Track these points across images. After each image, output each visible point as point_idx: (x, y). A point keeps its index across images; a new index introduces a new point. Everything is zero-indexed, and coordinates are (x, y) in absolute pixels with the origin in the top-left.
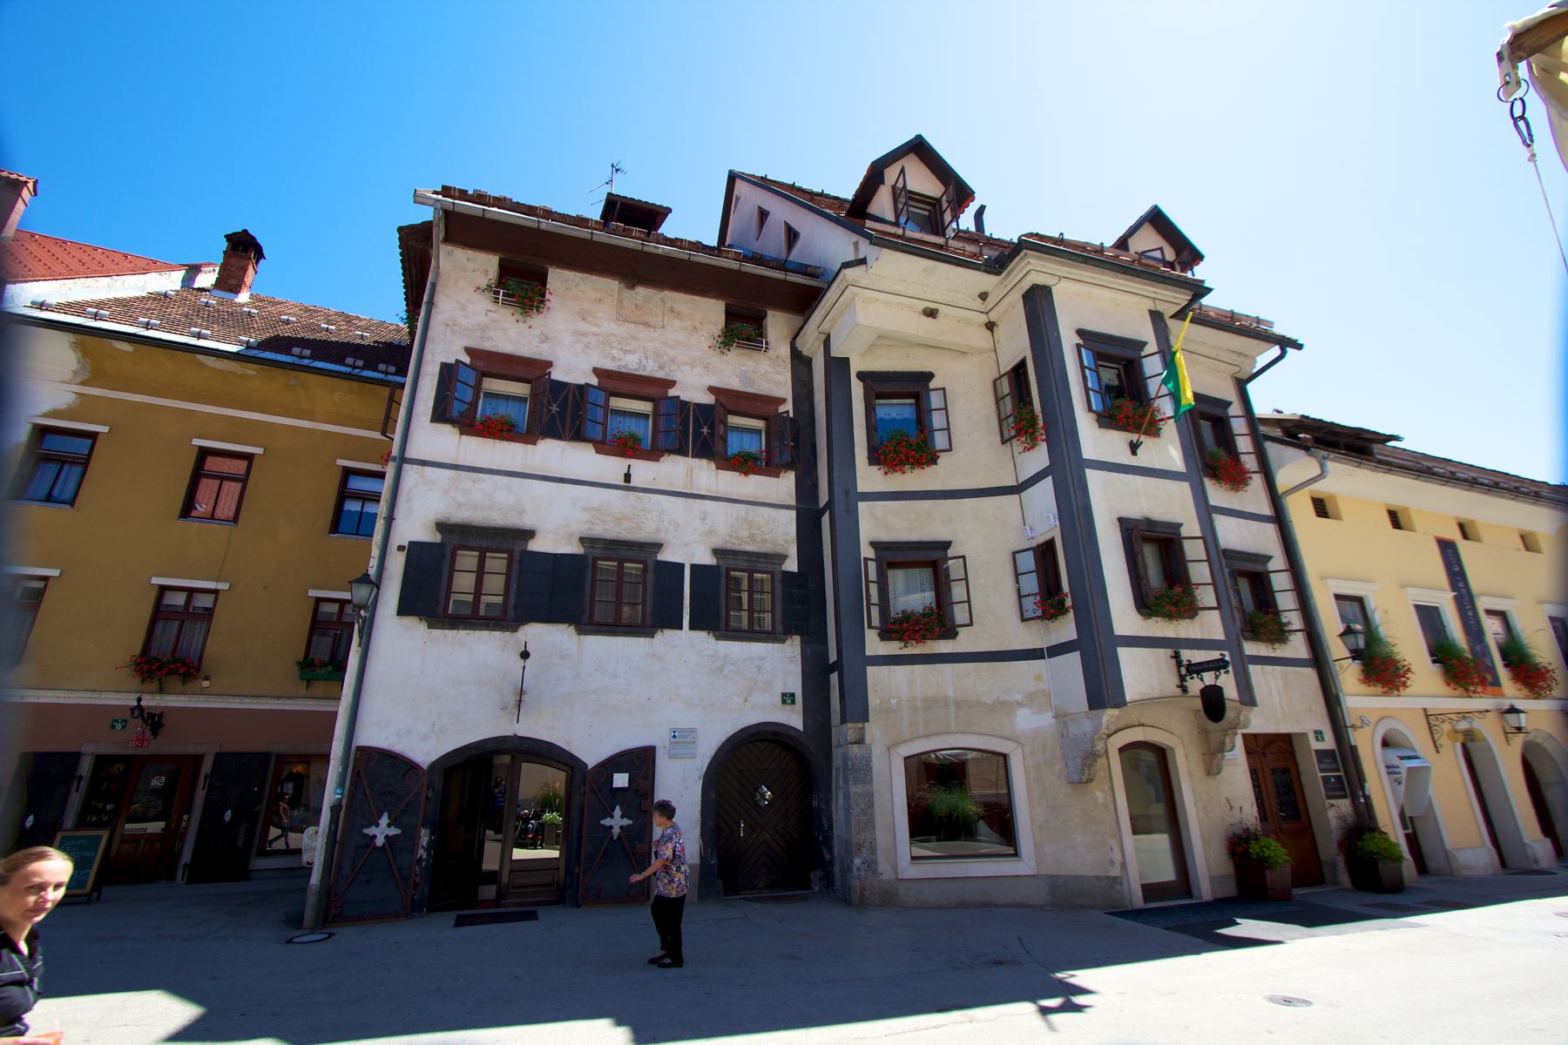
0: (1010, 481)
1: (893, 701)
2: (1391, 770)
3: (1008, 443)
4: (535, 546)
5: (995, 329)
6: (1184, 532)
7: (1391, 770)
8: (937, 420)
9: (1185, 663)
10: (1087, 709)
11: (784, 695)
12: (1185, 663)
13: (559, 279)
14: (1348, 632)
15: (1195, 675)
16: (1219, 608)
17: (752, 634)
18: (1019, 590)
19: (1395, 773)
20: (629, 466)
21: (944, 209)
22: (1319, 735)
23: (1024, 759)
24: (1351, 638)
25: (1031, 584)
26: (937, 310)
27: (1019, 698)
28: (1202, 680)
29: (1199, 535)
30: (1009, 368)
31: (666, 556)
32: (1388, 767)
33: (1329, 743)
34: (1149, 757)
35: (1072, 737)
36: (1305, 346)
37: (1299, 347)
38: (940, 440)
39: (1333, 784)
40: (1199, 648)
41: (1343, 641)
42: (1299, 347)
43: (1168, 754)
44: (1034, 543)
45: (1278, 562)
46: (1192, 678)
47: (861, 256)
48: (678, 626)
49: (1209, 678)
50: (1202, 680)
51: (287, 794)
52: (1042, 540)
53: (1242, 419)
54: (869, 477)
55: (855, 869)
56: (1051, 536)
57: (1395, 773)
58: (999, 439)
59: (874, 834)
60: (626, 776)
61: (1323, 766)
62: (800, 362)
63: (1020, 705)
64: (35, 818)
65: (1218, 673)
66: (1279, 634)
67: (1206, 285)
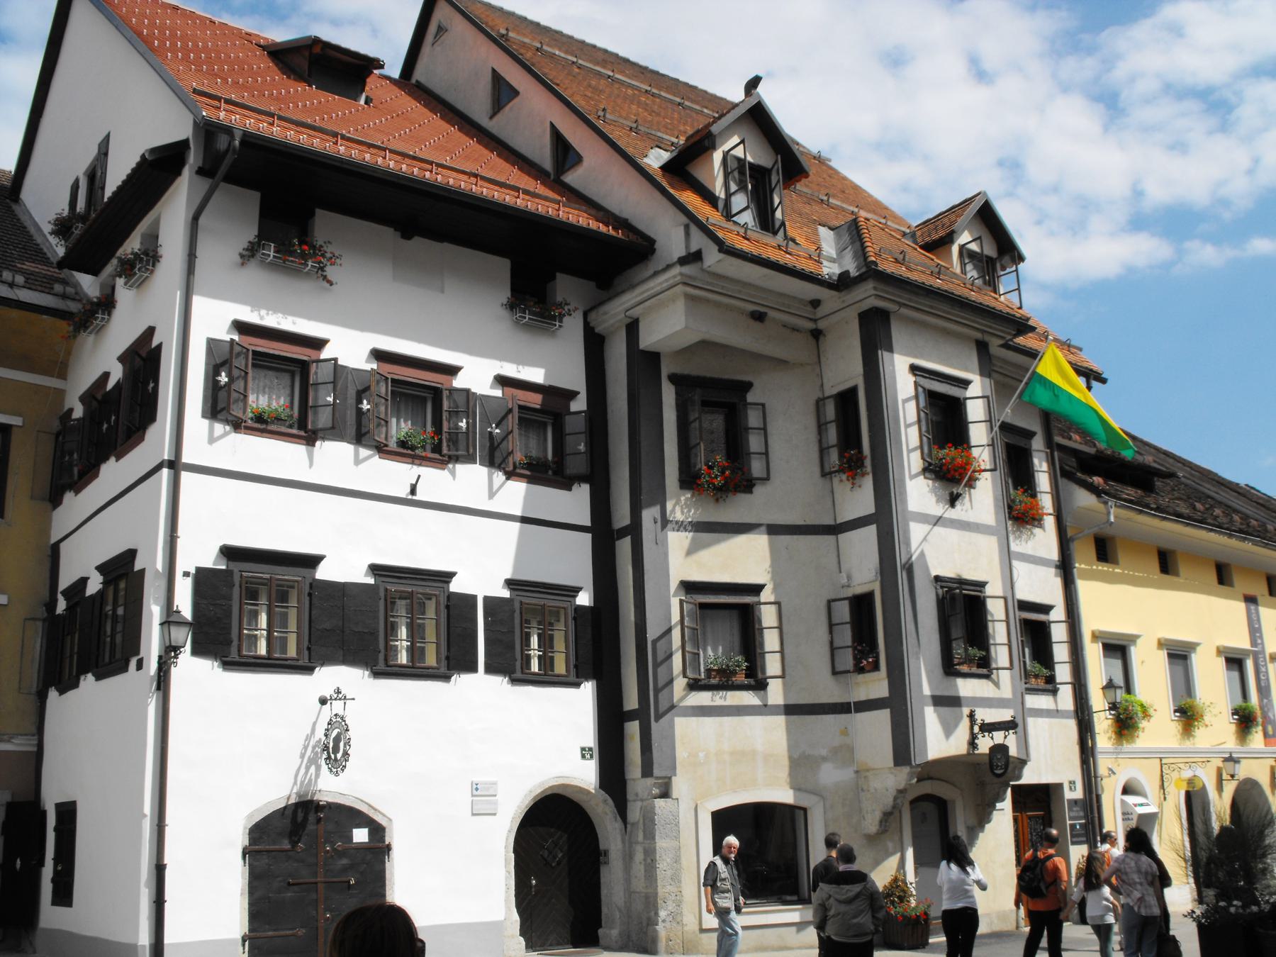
0: (828, 521)
1: (701, 755)
2: (1126, 816)
3: (828, 476)
4: (324, 573)
5: (821, 338)
6: (989, 590)
7: (1126, 816)
8: (755, 443)
9: (979, 721)
10: (891, 764)
11: (583, 749)
12: (979, 721)
13: (325, 224)
14: (1110, 686)
15: (986, 734)
16: (1011, 668)
17: (547, 679)
18: (831, 643)
19: (1129, 819)
20: (419, 476)
21: (773, 186)
22: (1072, 783)
23: (825, 813)
24: (1110, 692)
25: (845, 636)
26: (765, 314)
27: (824, 752)
28: (992, 738)
29: (1001, 594)
30: (835, 391)
31: (455, 586)
32: (1124, 814)
33: (1078, 794)
34: (929, 807)
35: (873, 791)
36: (1109, 382)
37: (1104, 381)
38: (757, 468)
39: (1078, 830)
40: (990, 706)
41: (1104, 693)
42: (1104, 381)
43: (949, 807)
44: (850, 593)
45: (1058, 614)
46: (984, 736)
47: (694, 249)
48: (472, 668)
49: (999, 737)
50: (992, 738)
51: (1257, 903)
52: (859, 590)
53: (1052, 517)
54: (680, 506)
55: (660, 921)
56: (871, 589)
57: (1129, 819)
58: (817, 470)
59: (680, 887)
60: (355, 831)
61: (1073, 814)
62: (595, 346)
63: (824, 759)
64: (15, 868)
65: (1007, 733)
66: (1050, 685)
67: (1030, 323)
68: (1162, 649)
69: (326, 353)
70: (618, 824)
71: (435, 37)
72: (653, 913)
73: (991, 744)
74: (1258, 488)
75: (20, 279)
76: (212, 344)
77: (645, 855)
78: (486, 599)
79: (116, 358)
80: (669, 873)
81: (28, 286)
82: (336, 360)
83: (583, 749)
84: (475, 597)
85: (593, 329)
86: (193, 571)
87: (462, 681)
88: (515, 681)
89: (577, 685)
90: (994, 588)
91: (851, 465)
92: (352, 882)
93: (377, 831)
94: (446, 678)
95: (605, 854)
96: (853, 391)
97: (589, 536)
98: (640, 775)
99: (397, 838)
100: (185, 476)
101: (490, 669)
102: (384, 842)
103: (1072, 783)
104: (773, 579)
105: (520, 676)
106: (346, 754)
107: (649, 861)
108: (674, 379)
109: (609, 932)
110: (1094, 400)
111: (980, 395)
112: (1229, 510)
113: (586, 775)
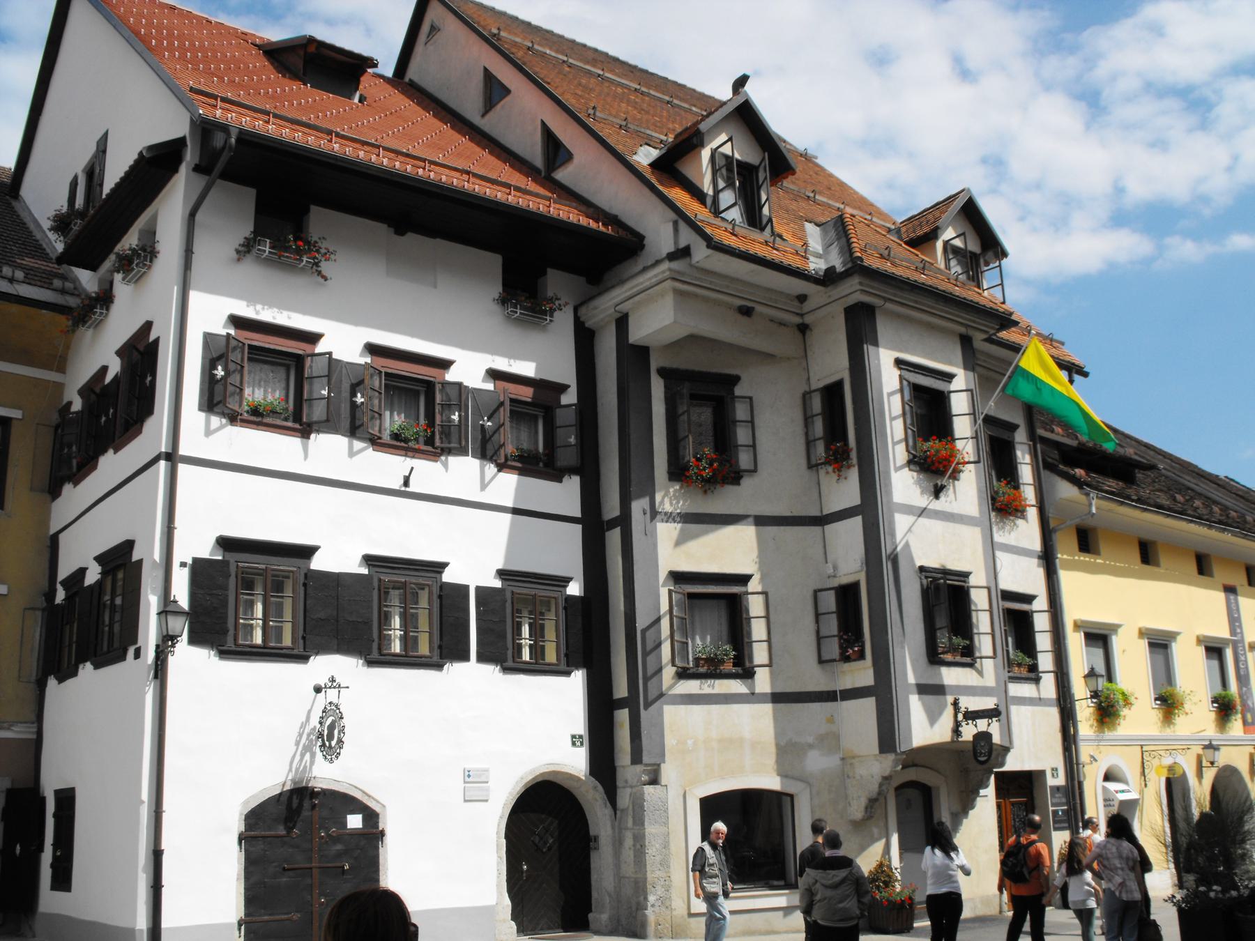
0: (814, 512)
1: (690, 742)
2: (1108, 803)
3: (815, 468)
4: (318, 563)
5: (808, 333)
6: (973, 581)
7: (1108, 803)
8: (742, 435)
9: (963, 709)
10: (877, 751)
11: (573, 737)
12: (963, 709)
13: (320, 221)
14: (1092, 674)
15: (970, 722)
16: (994, 657)
17: (538, 667)
18: (818, 632)
19: (1110, 805)
20: (412, 468)
21: (760, 183)
22: (1054, 770)
23: (811, 799)
24: (1092, 681)
25: (831, 625)
26: (753, 309)
27: (810, 740)
28: (976, 726)
29: (985, 584)
30: (821, 384)
31: (448, 577)
32: (1105, 800)
33: (1060, 781)
34: (913, 794)
35: (858, 777)
36: (1090, 375)
37: (1085, 375)
38: (744, 460)
39: (1060, 816)
40: (974, 695)
41: (1086, 682)
42: (1085, 375)
43: (934, 793)
44: (836, 583)
45: (1041, 604)
46: (967, 724)
47: (682, 244)
48: (464, 657)
49: (982, 725)
50: (976, 726)
51: (1236, 888)
52: (845, 580)
53: (1035, 508)
54: (669, 497)
55: (649, 905)
56: (857, 579)
57: (1110, 805)
58: (803, 462)
59: (669, 872)
60: (349, 817)
61: (1055, 801)
62: (585, 340)
63: (811, 746)
64: (15, 853)
65: (990, 721)
66: (1033, 674)
67: (1013, 317)
68: (1143, 638)
69: (321, 348)
70: (608, 811)
71: (428, 37)
72: (642, 898)
73: (975, 731)
74: (1237, 480)
75: (19, 275)
76: (209, 338)
77: (634, 841)
78: (478, 589)
79: (114, 352)
80: (658, 858)
81: (27, 281)
82: (330, 354)
83: (573, 737)
84: (467, 587)
85: (583, 323)
86: (190, 561)
87: (455, 670)
88: (506, 670)
89: (568, 674)
90: (978, 579)
91: (837, 458)
92: (347, 867)
93: (371, 817)
94: (439, 667)
95: (595, 839)
96: (839, 385)
97: (579, 527)
98: (629, 762)
99: (390, 824)
100: (182, 468)
101: (482, 658)
102: (378, 828)
103: (1054, 770)
104: (761, 569)
105: (512, 665)
106: (340, 741)
107: (638, 846)
108: (663, 372)
109: (599, 916)
110: (1076, 393)
111: (964, 388)
112: (1209, 501)
113: (576, 762)
